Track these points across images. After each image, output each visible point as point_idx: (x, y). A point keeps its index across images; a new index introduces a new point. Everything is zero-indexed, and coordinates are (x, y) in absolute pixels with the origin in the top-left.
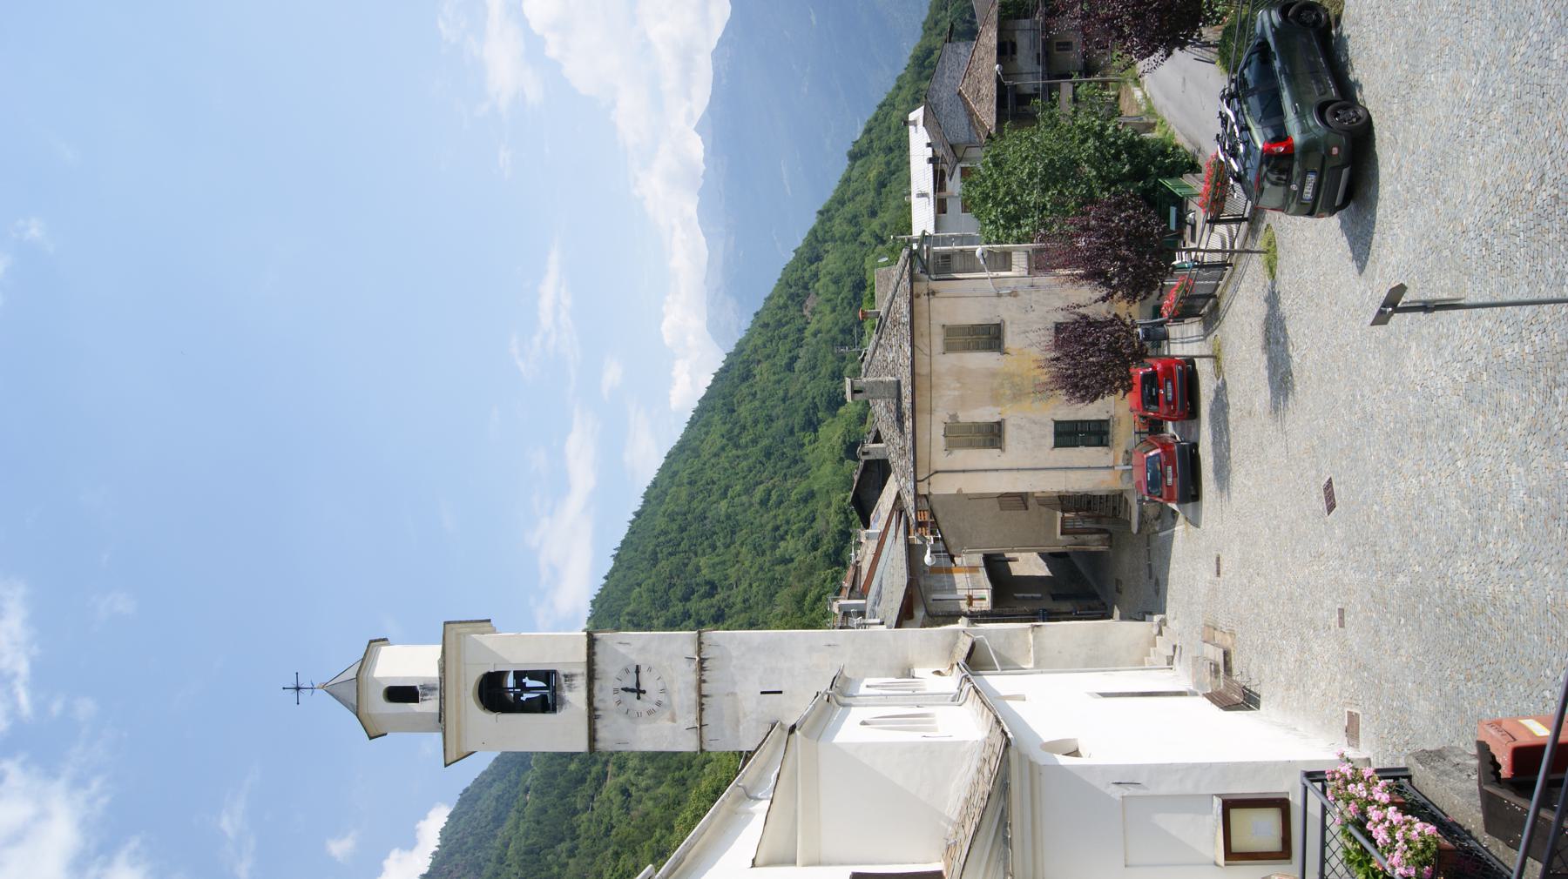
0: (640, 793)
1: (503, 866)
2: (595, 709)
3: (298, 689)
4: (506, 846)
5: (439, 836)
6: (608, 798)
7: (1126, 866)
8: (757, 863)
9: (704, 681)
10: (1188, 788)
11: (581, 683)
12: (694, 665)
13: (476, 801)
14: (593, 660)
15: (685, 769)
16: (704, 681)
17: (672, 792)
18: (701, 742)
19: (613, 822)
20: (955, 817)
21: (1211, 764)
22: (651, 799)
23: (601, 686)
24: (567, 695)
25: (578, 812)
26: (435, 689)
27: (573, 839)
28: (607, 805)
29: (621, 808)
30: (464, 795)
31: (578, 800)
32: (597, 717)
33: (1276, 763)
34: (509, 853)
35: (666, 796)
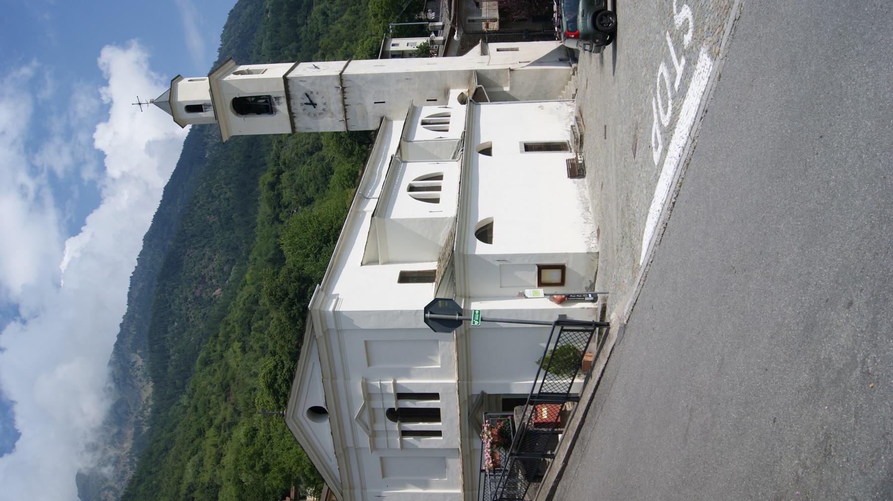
0: (334, 14)
1: (260, 56)
2: (293, 113)
3: (140, 104)
4: (261, 44)
5: (220, 39)
6: (315, 18)
7: (501, 287)
8: (364, 263)
9: (346, 98)
10: (526, 262)
11: (283, 101)
12: (339, 91)
13: (238, 18)
14: (288, 90)
15: (357, 5)
16: (346, 98)
17: (351, 18)
18: (347, 127)
19: (319, 31)
20: (443, 246)
21: (535, 254)
22: (339, 23)
23: (294, 102)
24: (278, 107)
25: (299, 26)
26: (210, 106)
27: (297, 42)
28: (315, 21)
29: (323, 23)
30: (231, 14)
31: (298, 19)
32: (294, 117)
33: (561, 254)
34: (263, 49)
35: (348, 21)
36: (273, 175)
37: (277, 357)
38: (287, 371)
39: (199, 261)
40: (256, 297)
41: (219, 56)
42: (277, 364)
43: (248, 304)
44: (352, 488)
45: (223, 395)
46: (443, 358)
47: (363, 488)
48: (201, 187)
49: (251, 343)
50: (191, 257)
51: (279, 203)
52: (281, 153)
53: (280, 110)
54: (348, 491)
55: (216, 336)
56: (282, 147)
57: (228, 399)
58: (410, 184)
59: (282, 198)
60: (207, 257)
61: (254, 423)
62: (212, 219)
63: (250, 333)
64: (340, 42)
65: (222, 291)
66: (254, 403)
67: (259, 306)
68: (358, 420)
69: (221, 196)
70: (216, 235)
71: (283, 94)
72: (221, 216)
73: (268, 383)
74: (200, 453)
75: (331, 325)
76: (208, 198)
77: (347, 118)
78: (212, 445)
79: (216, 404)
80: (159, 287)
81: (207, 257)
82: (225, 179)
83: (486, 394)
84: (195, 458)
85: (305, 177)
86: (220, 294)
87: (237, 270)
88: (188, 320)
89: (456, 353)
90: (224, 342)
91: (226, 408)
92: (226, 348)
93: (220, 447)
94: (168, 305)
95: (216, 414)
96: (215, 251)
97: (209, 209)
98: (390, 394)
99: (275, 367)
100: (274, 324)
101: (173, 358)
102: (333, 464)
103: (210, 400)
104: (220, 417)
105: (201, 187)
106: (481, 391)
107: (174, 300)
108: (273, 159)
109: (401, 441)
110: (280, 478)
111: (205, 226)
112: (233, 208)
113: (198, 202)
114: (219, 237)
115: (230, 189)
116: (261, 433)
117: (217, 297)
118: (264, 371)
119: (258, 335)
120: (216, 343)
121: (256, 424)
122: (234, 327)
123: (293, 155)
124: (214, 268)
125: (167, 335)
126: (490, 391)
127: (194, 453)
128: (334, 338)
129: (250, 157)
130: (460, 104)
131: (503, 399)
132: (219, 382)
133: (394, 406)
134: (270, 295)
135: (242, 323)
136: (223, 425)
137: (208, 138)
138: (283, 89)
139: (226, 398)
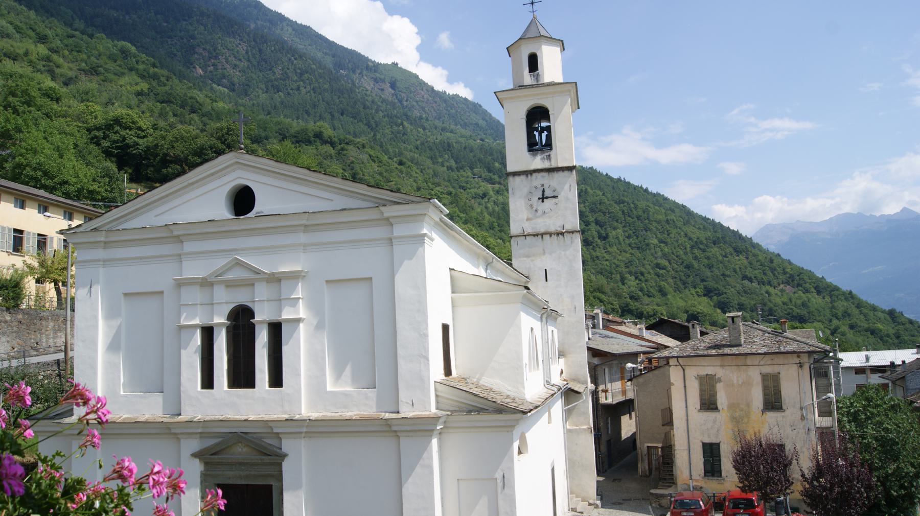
2: (531, 174)
4: (452, 132)
9: (551, 236)
11: (546, 165)
12: (559, 229)
13: (475, 112)
16: (551, 236)
17: (486, 222)
22: (482, 210)
26: (537, 81)
27: (457, 168)
28: (477, 186)
31: (478, 169)
32: (527, 176)
34: (447, 134)
35: (484, 219)
36: (330, 137)
37: (151, 131)
38: (135, 142)
39: (233, 54)
40: (199, 111)
41: (438, 91)
42: (143, 131)
43: (191, 102)
44: (106, 245)
45: (87, 68)
46: (345, 394)
47: (106, 262)
48: (311, 63)
49: (146, 102)
50: (237, 46)
51: (300, 141)
52: (352, 146)
53: (535, 161)
54: (102, 239)
55: (154, 66)
56: (358, 148)
57: (82, 72)
59: (307, 145)
60: (238, 63)
61: (66, 100)
62: (278, 71)
63: (158, 101)
64: (464, 211)
65: (201, 76)
66: (88, 101)
67: (189, 114)
68: (235, 262)
69: (302, 83)
70: (261, 75)
71: (554, 165)
72: (281, 81)
73: (122, 119)
74: (17, 36)
75: (399, 230)
76: (299, 69)
77: (527, 237)
78: (27, 50)
79: (77, 59)
80: (206, 11)
81: (238, 63)
82: (320, 88)
83: (283, 460)
84: (11, 29)
85: (330, 170)
86: (197, 73)
87: (224, 93)
88: (170, 37)
89: (358, 417)
90: (148, 74)
91: (71, 69)
92: (141, 74)
93: (25, 59)
94: (186, 18)
95: (64, 57)
96: (245, 72)
97: (288, 69)
98: (280, 312)
99: (140, 128)
100: (191, 130)
101: (127, 17)
102: (150, 219)
103: (81, 52)
104: (61, 61)
105: (311, 63)
106: (287, 453)
107: (191, 25)
108: (346, 139)
109: (194, 327)
110: (9, 126)
111: (270, 63)
112: (289, 94)
113: (296, 59)
114: (258, 77)
115: (309, 92)
116: (55, 106)
117: (194, 70)
118: (135, 116)
119: (157, 111)
120: (147, 64)
121: (65, 101)
122: (165, 85)
123: (351, 158)
124: (225, 69)
125: (153, 14)
126: (286, 466)
127: (17, 28)
128: (380, 232)
129: (342, 114)
131: (272, 485)
132: (103, 64)
133: (258, 317)
134: (228, 129)
135: (170, 94)
136: (51, 64)
137: (360, 74)
138: (560, 165)
139: (84, 71)
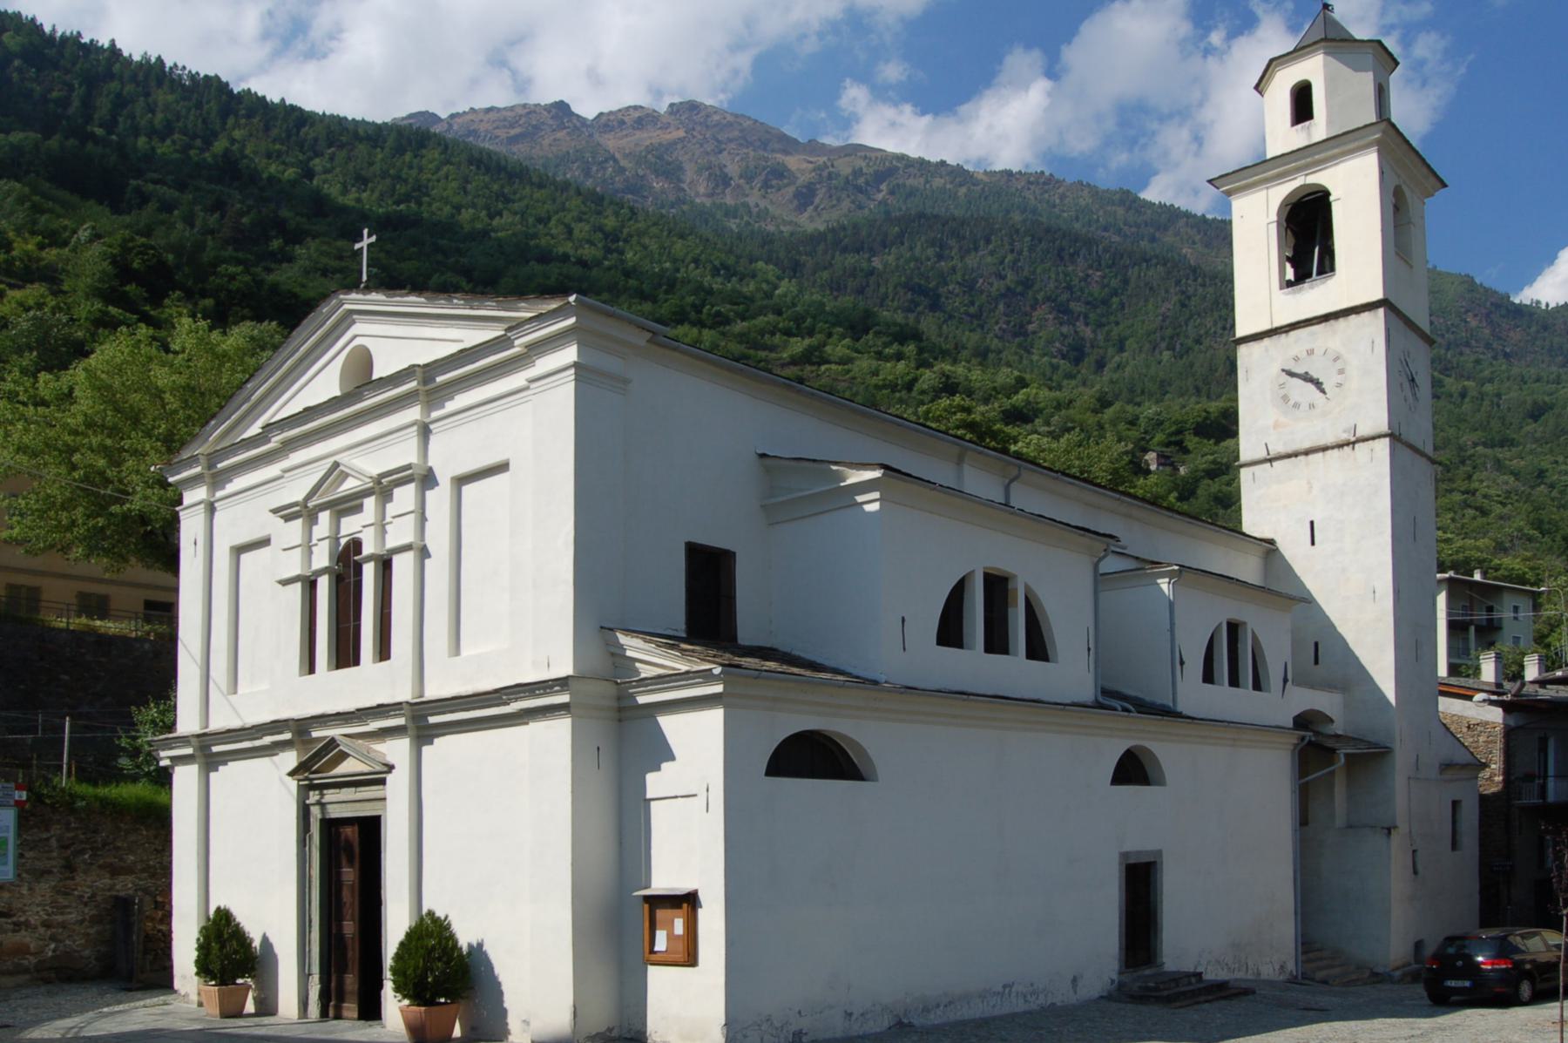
58: (1245, 623)
130: (1296, 714)
